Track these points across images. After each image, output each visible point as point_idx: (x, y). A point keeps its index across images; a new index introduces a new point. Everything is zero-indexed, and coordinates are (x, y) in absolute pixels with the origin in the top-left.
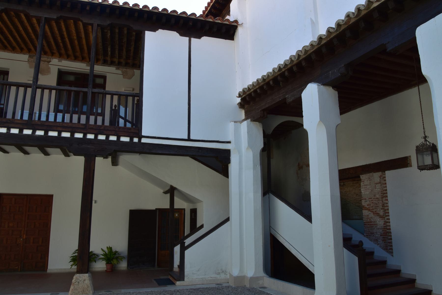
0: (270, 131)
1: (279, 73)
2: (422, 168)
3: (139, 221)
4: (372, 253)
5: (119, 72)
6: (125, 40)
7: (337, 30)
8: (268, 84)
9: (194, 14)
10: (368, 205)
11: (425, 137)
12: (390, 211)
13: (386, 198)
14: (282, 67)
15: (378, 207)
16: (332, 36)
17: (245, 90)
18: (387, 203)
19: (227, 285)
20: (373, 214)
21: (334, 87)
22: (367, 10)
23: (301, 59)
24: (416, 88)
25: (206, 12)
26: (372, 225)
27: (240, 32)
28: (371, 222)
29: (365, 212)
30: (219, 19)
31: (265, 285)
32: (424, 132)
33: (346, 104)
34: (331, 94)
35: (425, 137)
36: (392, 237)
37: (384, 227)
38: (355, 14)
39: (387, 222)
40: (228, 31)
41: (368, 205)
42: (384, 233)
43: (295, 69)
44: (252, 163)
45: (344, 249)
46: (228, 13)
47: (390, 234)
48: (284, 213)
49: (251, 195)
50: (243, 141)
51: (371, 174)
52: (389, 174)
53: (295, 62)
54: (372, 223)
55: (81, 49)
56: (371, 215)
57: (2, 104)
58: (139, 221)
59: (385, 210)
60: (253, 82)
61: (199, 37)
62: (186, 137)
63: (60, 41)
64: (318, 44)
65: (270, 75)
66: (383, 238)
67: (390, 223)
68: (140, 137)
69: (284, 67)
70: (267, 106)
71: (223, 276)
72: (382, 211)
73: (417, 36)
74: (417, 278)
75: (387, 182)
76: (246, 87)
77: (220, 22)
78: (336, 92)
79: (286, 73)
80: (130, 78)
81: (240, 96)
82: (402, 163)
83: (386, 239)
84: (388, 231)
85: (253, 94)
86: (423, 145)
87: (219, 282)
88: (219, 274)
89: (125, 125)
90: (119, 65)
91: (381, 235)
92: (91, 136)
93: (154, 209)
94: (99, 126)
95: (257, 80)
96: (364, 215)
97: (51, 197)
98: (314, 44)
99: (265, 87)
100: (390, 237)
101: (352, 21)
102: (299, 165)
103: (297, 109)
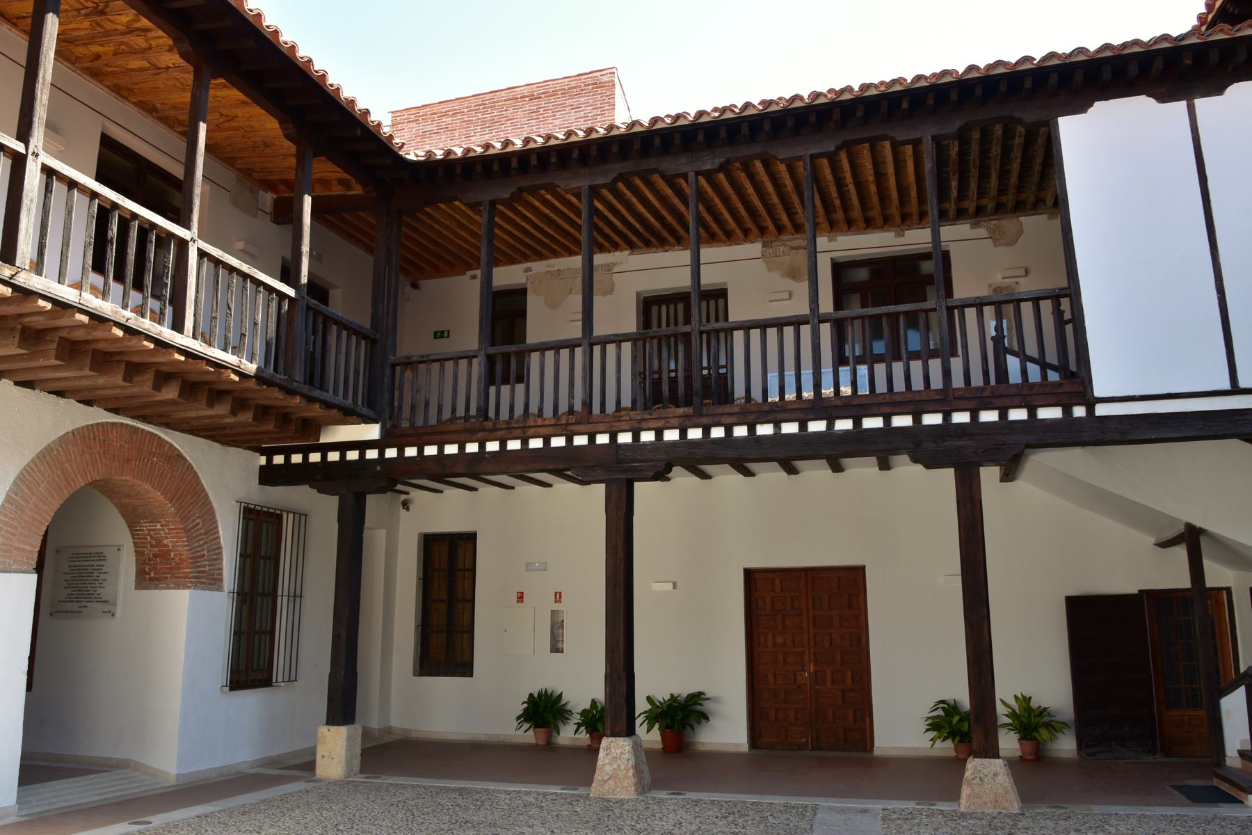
3: (1095, 624)
5: (981, 232)
6: (996, 150)
55: (883, 198)
57: (723, 367)
58: (1095, 624)
61: (1219, 90)
62: (1226, 385)
63: (835, 195)
68: (1091, 402)
80: (1012, 243)
89: (1044, 376)
90: (978, 215)
92: (961, 418)
93: (1135, 591)
94: (977, 389)
97: (859, 572)
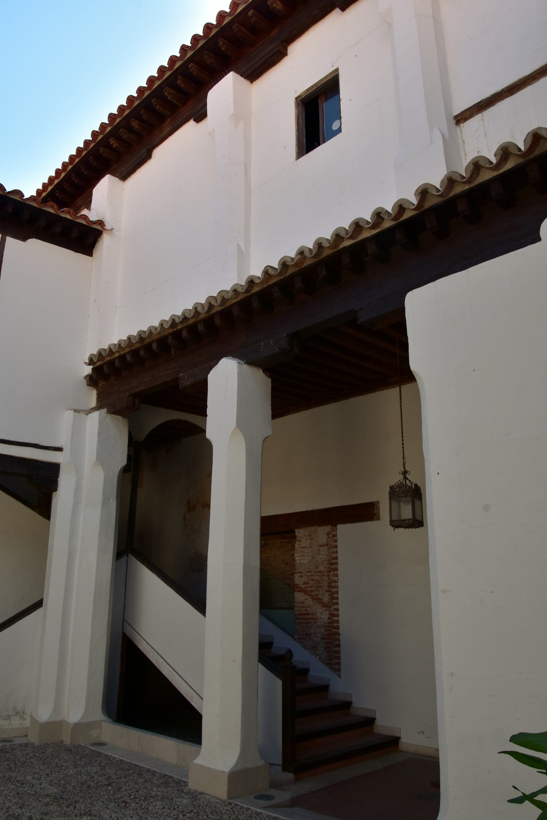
0: (142, 436)
1: (171, 331)
2: (396, 524)
4: (305, 671)
7: (280, 274)
8: (148, 347)
9: (18, 192)
10: (304, 584)
11: (405, 473)
12: (340, 596)
13: (335, 572)
14: (177, 321)
15: (321, 587)
16: (271, 282)
17: (103, 353)
18: (336, 582)
19: (23, 741)
20: (313, 599)
21: (267, 370)
22: (333, 248)
23: (213, 311)
24: (398, 388)
25: (44, 194)
26: (310, 619)
27: (105, 243)
28: (308, 614)
29: (299, 597)
30: (69, 212)
31: (104, 739)
32: (404, 464)
33: (283, 402)
34: (260, 382)
35: (405, 473)
36: (342, 642)
37: (329, 623)
38: (314, 253)
39: (334, 615)
40: (84, 238)
41: (304, 584)
42: (328, 635)
43: (201, 327)
44: (100, 492)
45: (260, 665)
46: (88, 204)
47: (337, 637)
48: (155, 593)
49: (93, 557)
50: (88, 451)
51: (313, 528)
52: (343, 529)
53: (202, 316)
54: (310, 616)
56: (309, 601)
59: (333, 594)
60: (120, 341)
61: (24, 238)
64: (247, 291)
65: (153, 331)
66: (326, 643)
67: (338, 616)
69: (182, 322)
70: (142, 388)
71: (16, 723)
72: (327, 594)
73: (406, 306)
74: (378, 716)
75: (339, 544)
76: (106, 347)
77: (69, 217)
78: (269, 380)
79: (185, 334)
81: (91, 362)
82: (365, 512)
83: (330, 645)
84: (334, 630)
85: (117, 363)
86: (401, 485)
87: (6, 736)
88: (8, 717)
91: (322, 639)
95: (129, 338)
96: (296, 600)
98: (240, 290)
99: (142, 352)
100: (336, 642)
101: (308, 263)
102: (189, 503)
103: (196, 400)
